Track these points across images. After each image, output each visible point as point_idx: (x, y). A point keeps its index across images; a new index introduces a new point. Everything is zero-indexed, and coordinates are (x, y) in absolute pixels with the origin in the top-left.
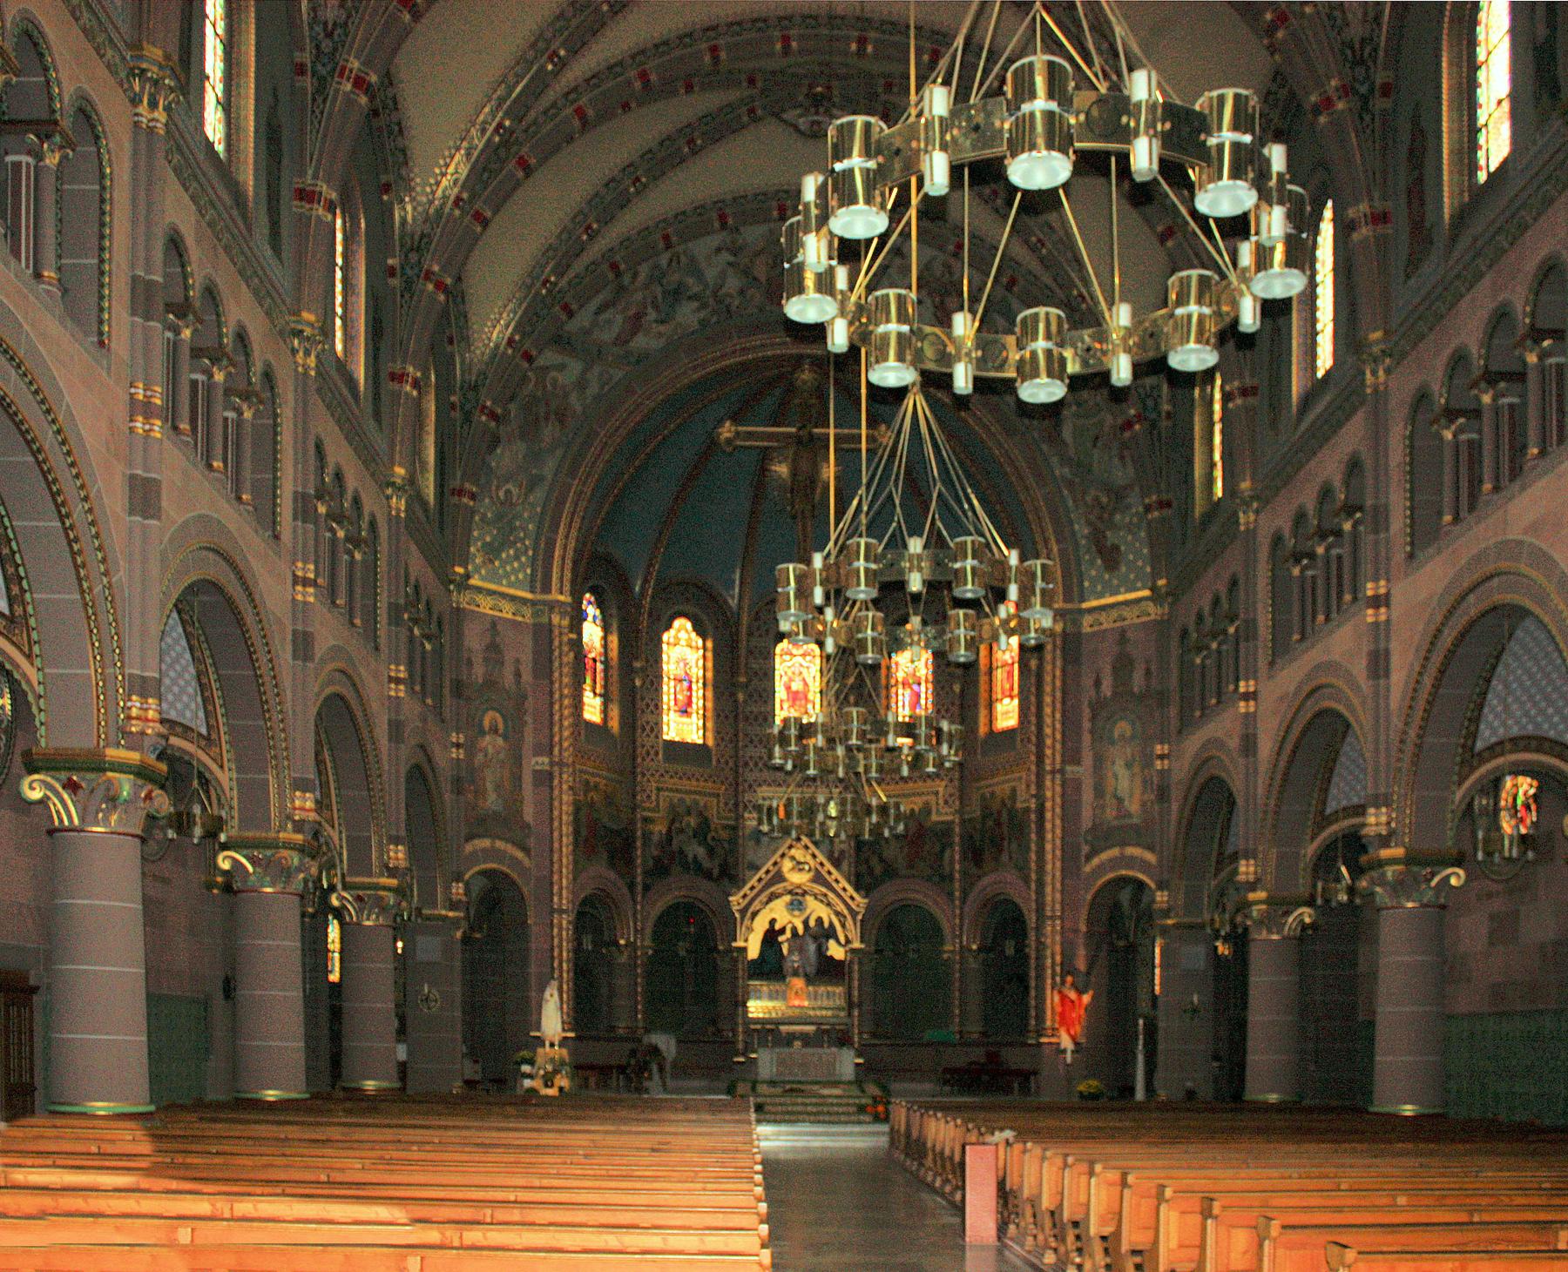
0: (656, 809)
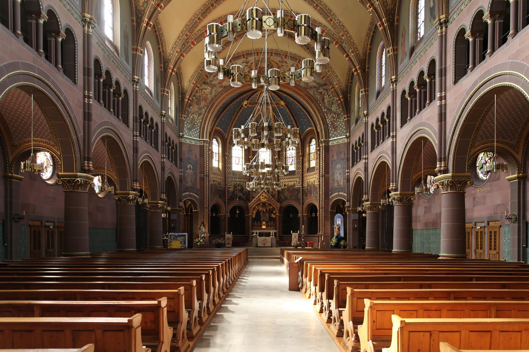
0: (231, 185)
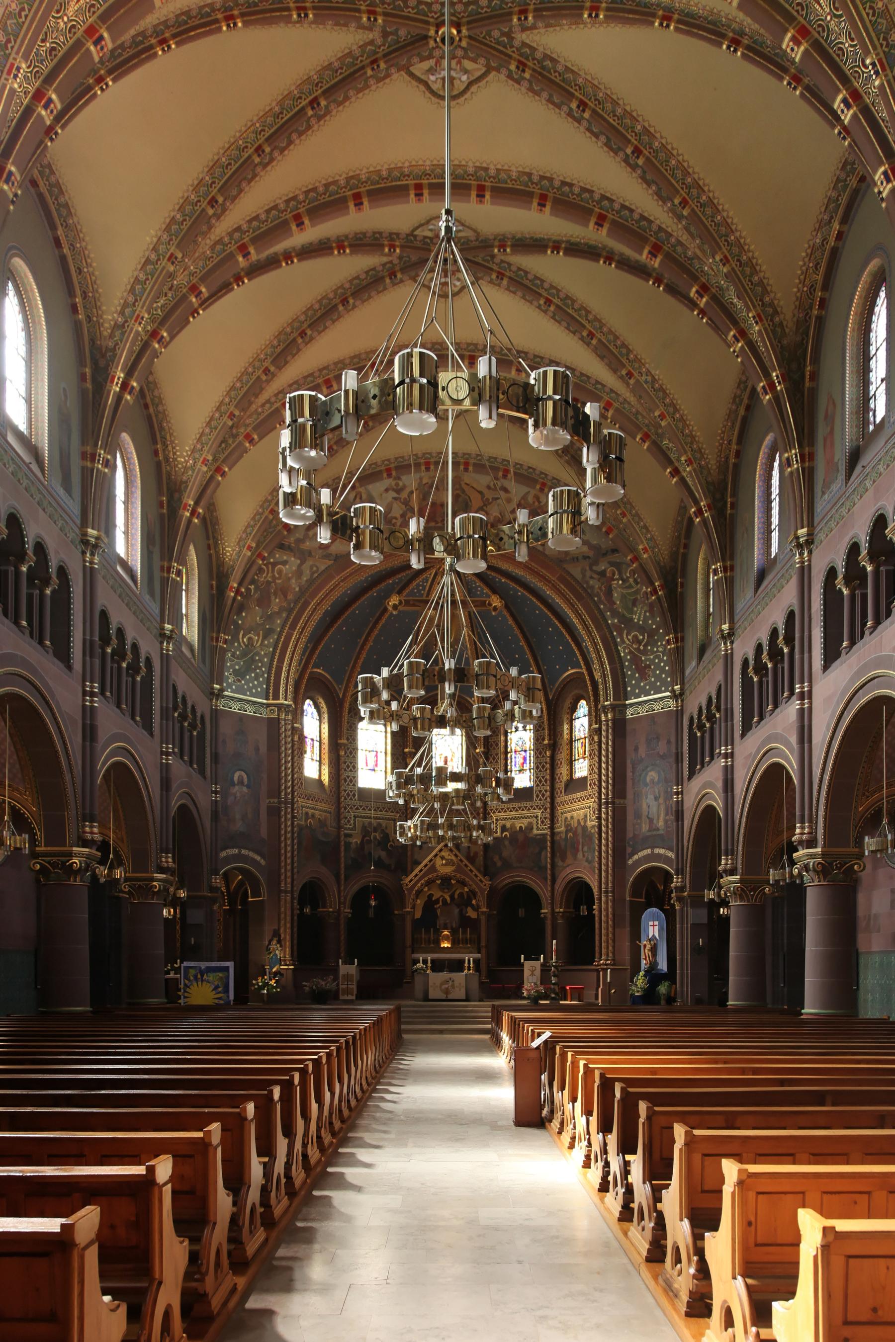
0: (354, 829)
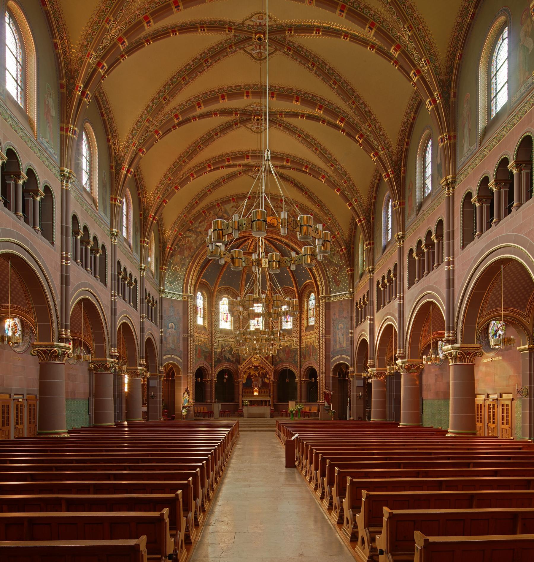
0: (218, 346)
